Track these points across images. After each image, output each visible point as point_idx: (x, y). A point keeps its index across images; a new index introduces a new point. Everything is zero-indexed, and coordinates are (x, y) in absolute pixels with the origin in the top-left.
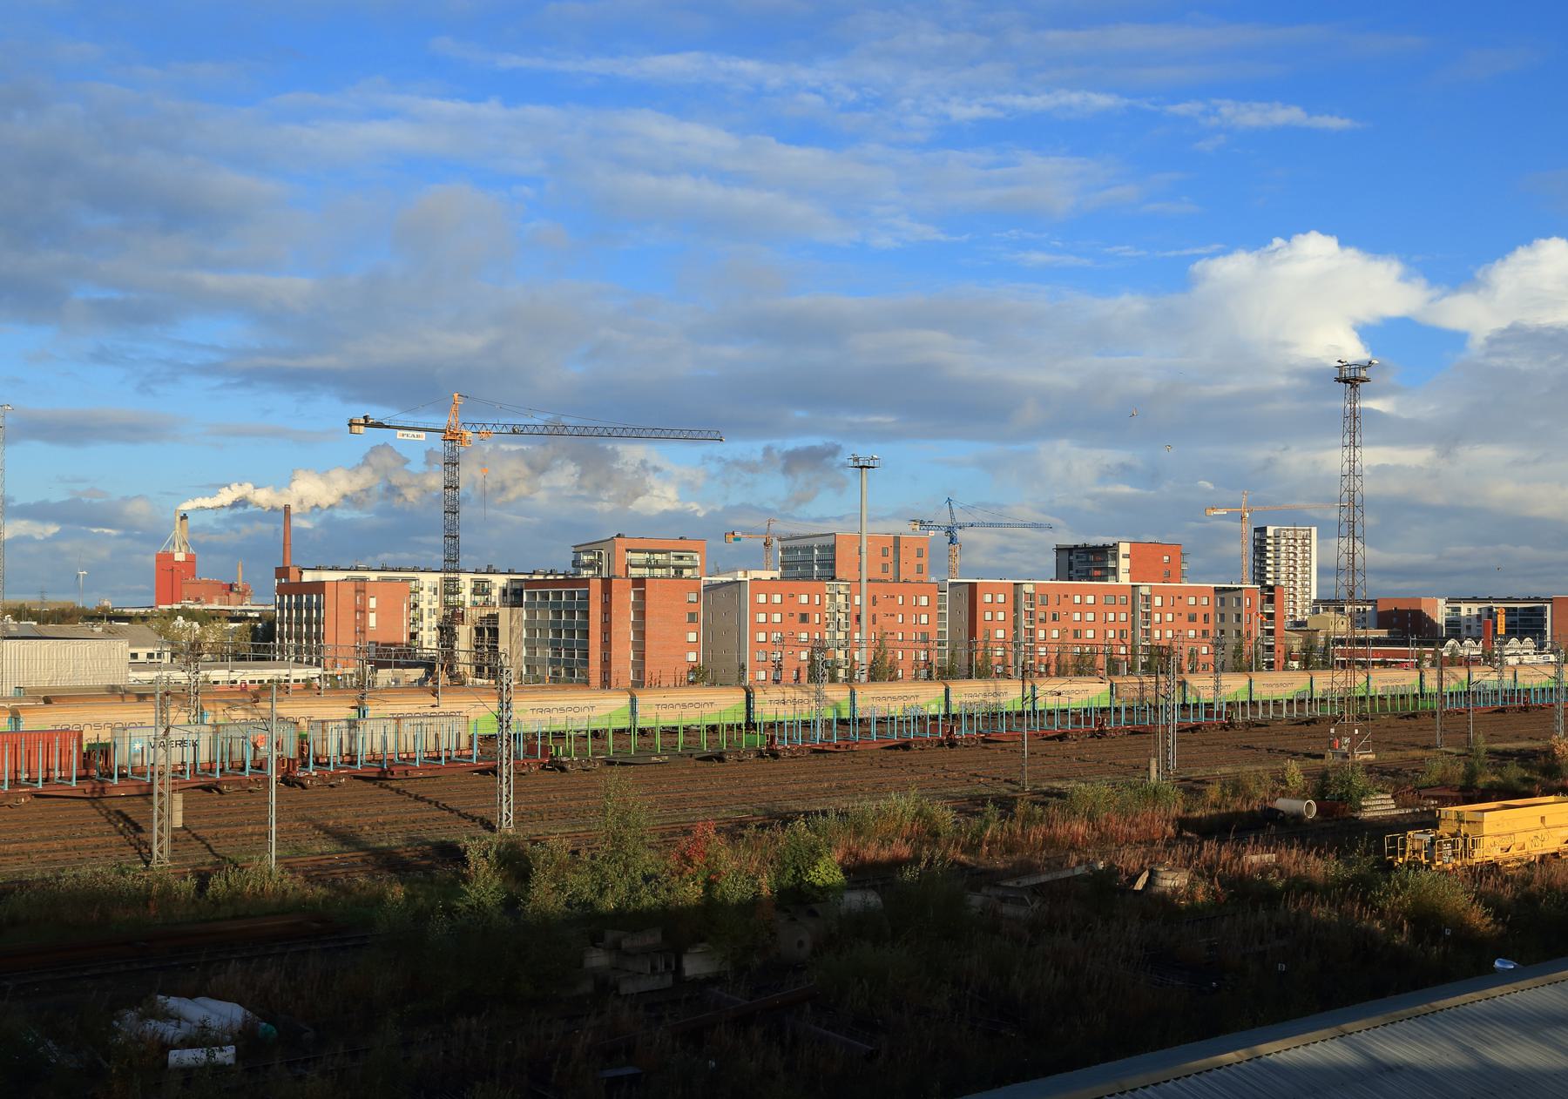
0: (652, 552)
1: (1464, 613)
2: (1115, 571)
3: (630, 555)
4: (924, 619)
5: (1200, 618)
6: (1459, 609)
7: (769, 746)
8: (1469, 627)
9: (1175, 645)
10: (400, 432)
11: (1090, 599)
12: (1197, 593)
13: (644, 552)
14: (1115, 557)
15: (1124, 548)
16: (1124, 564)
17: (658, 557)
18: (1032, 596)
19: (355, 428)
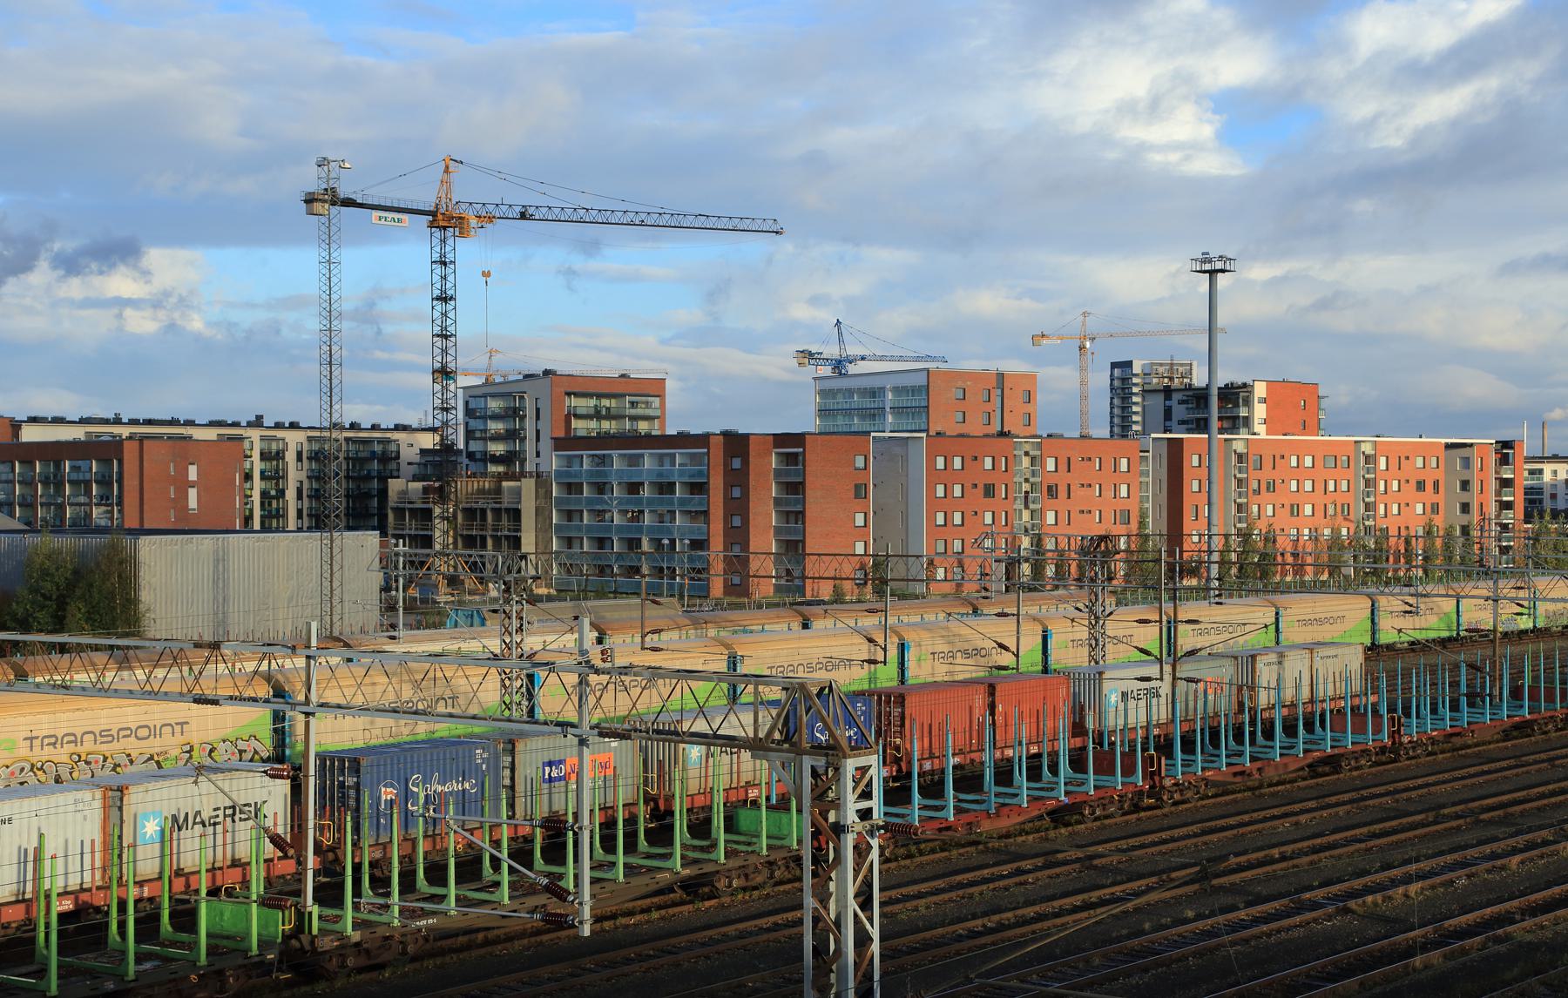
0: (599, 396)
1: (1547, 477)
2: (1247, 422)
3: (574, 402)
4: (1124, 491)
5: (1429, 486)
6: (1541, 471)
7: (1478, 636)
8: (1553, 496)
9: (1277, 527)
10: (376, 214)
11: (1308, 461)
12: (1425, 451)
13: (590, 395)
14: (1248, 402)
15: (1260, 390)
16: (1260, 411)
17: (606, 402)
18: (1240, 457)
19: (318, 207)
